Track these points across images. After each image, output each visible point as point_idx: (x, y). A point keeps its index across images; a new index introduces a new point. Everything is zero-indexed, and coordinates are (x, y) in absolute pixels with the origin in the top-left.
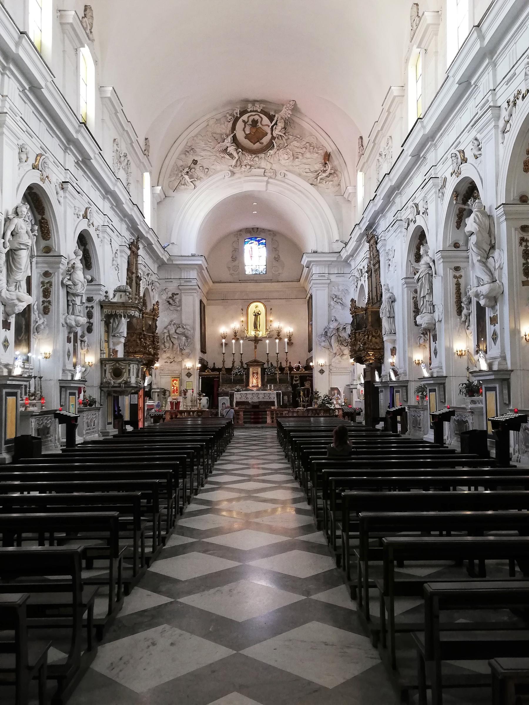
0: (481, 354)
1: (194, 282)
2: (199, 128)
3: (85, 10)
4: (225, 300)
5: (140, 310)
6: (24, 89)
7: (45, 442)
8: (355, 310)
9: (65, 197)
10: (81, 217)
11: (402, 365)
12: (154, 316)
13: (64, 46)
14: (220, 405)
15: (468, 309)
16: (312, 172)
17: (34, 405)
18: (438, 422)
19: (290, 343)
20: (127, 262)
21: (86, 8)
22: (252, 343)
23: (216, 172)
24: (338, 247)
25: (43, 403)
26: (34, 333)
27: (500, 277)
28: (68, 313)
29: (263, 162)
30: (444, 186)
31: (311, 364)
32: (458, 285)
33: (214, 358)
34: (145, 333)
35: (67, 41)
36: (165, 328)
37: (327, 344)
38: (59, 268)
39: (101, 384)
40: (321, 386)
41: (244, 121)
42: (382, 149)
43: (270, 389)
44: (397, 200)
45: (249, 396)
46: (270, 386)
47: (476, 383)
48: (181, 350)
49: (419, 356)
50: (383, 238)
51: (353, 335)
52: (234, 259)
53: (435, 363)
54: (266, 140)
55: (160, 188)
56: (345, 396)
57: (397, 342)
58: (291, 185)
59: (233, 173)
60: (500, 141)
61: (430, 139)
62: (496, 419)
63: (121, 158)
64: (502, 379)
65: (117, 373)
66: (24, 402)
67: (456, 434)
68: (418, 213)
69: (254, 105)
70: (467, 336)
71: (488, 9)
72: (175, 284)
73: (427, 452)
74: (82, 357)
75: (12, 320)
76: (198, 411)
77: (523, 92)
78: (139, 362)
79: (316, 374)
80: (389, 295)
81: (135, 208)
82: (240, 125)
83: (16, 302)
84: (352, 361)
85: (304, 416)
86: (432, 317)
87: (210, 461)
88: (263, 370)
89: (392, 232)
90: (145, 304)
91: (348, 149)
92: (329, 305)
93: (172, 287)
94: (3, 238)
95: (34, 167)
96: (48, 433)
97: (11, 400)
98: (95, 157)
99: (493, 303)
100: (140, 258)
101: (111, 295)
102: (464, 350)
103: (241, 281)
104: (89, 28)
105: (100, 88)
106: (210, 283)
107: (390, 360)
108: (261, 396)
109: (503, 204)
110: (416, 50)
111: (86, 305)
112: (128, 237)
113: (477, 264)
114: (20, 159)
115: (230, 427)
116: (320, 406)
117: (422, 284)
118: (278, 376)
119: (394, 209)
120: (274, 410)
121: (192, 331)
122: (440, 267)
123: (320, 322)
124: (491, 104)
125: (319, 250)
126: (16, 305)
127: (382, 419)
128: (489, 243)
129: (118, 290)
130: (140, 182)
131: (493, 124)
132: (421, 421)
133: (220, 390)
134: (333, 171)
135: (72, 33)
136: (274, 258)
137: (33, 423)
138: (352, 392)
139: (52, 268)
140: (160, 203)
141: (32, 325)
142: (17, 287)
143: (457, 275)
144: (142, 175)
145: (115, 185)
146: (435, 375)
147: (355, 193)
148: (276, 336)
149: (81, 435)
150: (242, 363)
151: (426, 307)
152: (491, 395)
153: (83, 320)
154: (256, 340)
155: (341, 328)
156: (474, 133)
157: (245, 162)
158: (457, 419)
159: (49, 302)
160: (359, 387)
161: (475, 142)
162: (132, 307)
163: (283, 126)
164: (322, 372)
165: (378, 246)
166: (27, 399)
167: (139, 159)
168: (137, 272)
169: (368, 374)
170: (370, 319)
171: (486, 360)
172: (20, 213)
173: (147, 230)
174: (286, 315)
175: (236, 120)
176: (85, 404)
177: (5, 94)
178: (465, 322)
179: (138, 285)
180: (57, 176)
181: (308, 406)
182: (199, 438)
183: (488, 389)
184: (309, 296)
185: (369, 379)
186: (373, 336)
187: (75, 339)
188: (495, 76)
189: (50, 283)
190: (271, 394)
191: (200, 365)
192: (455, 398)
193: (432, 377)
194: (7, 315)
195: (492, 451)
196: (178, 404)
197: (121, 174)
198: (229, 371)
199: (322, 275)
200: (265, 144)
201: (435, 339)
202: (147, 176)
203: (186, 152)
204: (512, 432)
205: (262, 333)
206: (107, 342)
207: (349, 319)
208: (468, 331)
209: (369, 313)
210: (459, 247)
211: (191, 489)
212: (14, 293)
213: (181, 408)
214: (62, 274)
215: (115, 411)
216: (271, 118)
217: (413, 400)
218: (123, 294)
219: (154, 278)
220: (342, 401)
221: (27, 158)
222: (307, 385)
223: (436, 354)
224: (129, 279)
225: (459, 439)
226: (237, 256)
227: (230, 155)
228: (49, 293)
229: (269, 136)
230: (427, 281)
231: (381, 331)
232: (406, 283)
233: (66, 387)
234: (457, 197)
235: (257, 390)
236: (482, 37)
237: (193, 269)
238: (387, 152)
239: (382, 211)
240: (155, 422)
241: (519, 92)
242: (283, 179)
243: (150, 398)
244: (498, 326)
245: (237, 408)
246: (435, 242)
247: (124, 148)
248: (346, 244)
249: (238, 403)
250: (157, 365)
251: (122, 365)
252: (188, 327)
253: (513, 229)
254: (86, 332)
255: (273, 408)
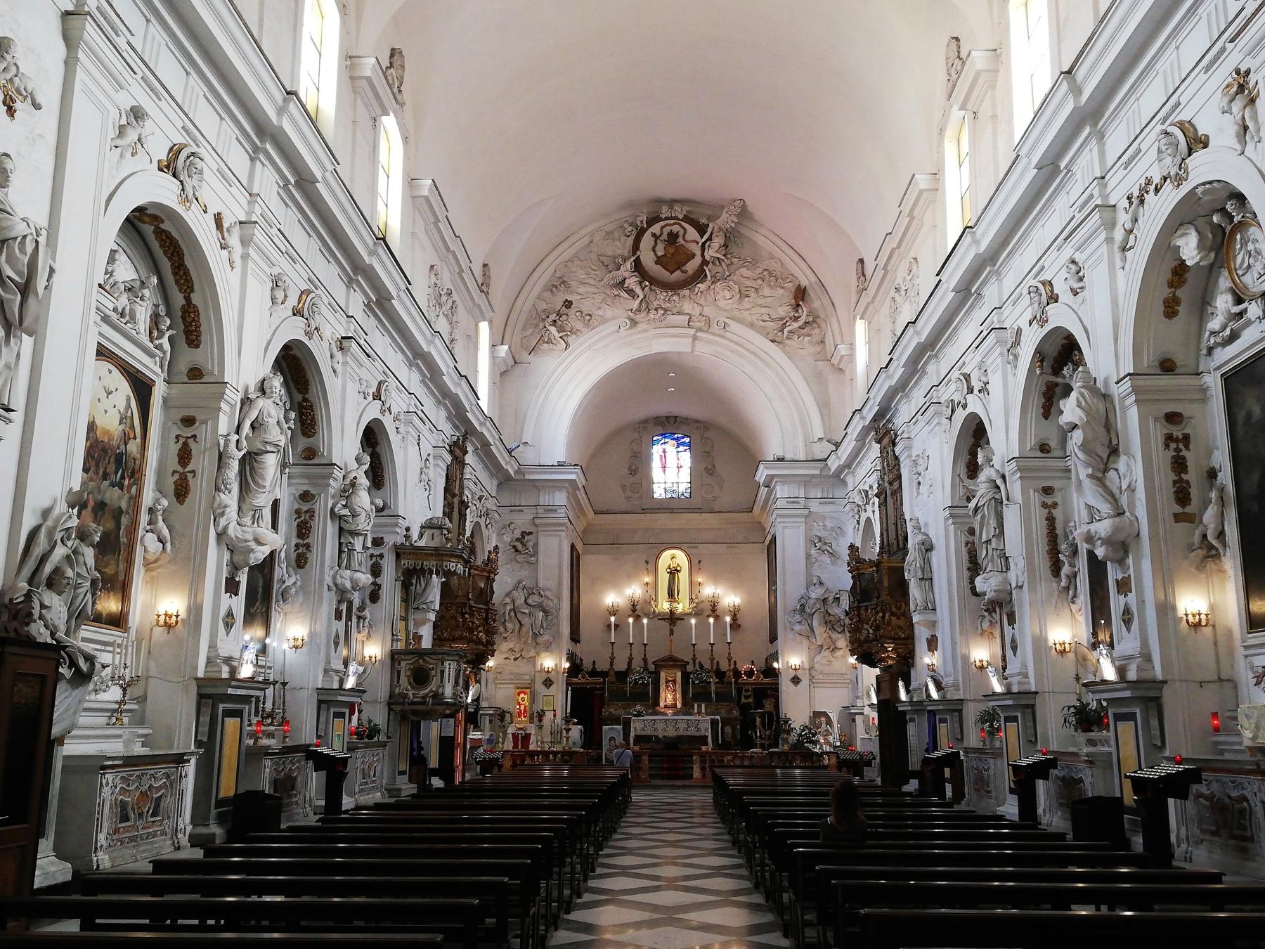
0: (1103, 650)
1: (562, 512)
2: (572, 251)
3: (392, 56)
4: (615, 543)
5: (466, 562)
6: (287, 182)
7: (287, 805)
8: (856, 563)
9: (345, 364)
10: (370, 398)
11: (950, 669)
12: (489, 572)
13: (355, 110)
14: (605, 742)
15: (1072, 565)
16: (773, 320)
17: (270, 735)
18: (1025, 780)
19: (735, 625)
20: (444, 475)
21: (393, 52)
22: (666, 625)
23: (604, 321)
24: (822, 450)
25: (285, 732)
26: (277, 601)
27: (1132, 504)
28: (339, 566)
29: (687, 304)
30: (1017, 343)
31: (775, 665)
32: (1051, 520)
33: (594, 652)
34: (472, 603)
35: (361, 109)
36: (508, 595)
37: (804, 627)
38: (329, 485)
39: (391, 697)
40: (796, 708)
41: (654, 235)
42: (899, 281)
43: (699, 713)
44: (931, 368)
45: (660, 726)
46: (700, 707)
47: (1094, 705)
48: (535, 636)
49: (981, 652)
50: (905, 435)
51: (855, 611)
52: (633, 471)
53: (1014, 666)
54: (691, 266)
55: (506, 347)
56: (841, 729)
57: (940, 625)
58: (736, 343)
59: (634, 323)
60: (1119, 264)
61: (988, 262)
62: (1140, 774)
63: (441, 296)
64: (1145, 697)
65: (420, 677)
66: (254, 728)
67: (1061, 804)
68: (971, 391)
69: (671, 207)
70: (1073, 616)
71: (1086, 45)
72: (528, 515)
73: (1005, 837)
74: (359, 647)
75: (243, 578)
76: (564, 753)
77: (1157, 180)
78: (461, 657)
79: (785, 685)
80: (920, 538)
81: (464, 383)
82: (647, 240)
83: (253, 545)
84: (852, 660)
85: (765, 765)
86: (1005, 579)
87: (591, 849)
88: (686, 676)
89: (921, 424)
90: (473, 551)
91: (840, 282)
92: (808, 556)
93: (522, 521)
94: (237, 432)
95: (296, 312)
96: (293, 788)
97: (232, 723)
98: (399, 296)
99: (1121, 553)
100: (467, 470)
101: (415, 536)
102: (1067, 641)
103: (644, 511)
104: (397, 84)
105: (411, 182)
106: (590, 514)
107: (926, 659)
108: (682, 726)
109: (1129, 374)
110: (957, 114)
111: (371, 551)
112: (448, 431)
113: (1087, 483)
114: (273, 299)
115: (624, 785)
116: (794, 746)
117: (983, 517)
118: (713, 688)
119: (925, 384)
120: (707, 752)
121: (556, 601)
122: (1015, 488)
123: (792, 586)
124: (1099, 202)
125: (788, 456)
126: (252, 550)
127: (914, 775)
128: (1106, 443)
129: (428, 526)
130: (473, 339)
131: (1103, 235)
132: (992, 779)
133: (605, 713)
134: (811, 319)
135: (370, 94)
136: (704, 470)
137: (268, 769)
138: (854, 720)
139: (315, 485)
140: (504, 374)
141: (276, 587)
142: (256, 519)
143: (1049, 501)
144: (477, 325)
145: (430, 342)
146: (1015, 689)
147: (852, 356)
148: (709, 612)
149: (351, 795)
150: (645, 660)
151: (992, 561)
152: (1126, 729)
153: (365, 578)
154: (673, 618)
155: (831, 599)
156: (1068, 252)
157: (655, 303)
158: (1061, 774)
159: (308, 546)
160: (867, 711)
161: (1071, 266)
162: (453, 556)
163: (722, 242)
164: (796, 680)
165: (898, 450)
166: (259, 724)
167: (472, 299)
168: (461, 494)
169: (885, 685)
170: (886, 583)
171: (1113, 662)
172: (268, 391)
173: (370, 242)
174: (730, 574)
175: (641, 233)
176: (360, 735)
177: (255, 191)
178: (1068, 588)
179: (462, 517)
180: (333, 327)
181: (770, 746)
182: (564, 802)
183: (1119, 717)
184: (769, 538)
185: (886, 696)
186: (892, 614)
187: (349, 611)
188: (1102, 154)
189: (311, 513)
190: (702, 722)
191: (567, 665)
192: (1055, 732)
193: (1009, 693)
194: (235, 568)
195: (1133, 839)
196: (527, 737)
197: (442, 325)
198: (622, 676)
199: (793, 500)
200: (690, 272)
201: (1012, 621)
202: (484, 327)
203: (552, 288)
204: (1171, 801)
205: (682, 606)
206: (405, 619)
207: (847, 581)
208: (1073, 607)
209: (885, 571)
210: (1049, 452)
211: (560, 900)
212: (249, 530)
213: (532, 747)
214: (333, 497)
215: (412, 750)
216: (701, 230)
217: (973, 738)
218: (437, 532)
219: (490, 504)
220: (835, 738)
221: (286, 296)
222: (768, 705)
223: (1014, 648)
224: (448, 506)
225: (1068, 816)
226: (638, 468)
227: (630, 292)
228: (309, 529)
229: (697, 260)
230: (993, 513)
231: (908, 604)
232: (952, 516)
233: (330, 702)
234: (1042, 361)
235: (674, 714)
236: (1076, 90)
237: (560, 488)
238: (909, 285)
239: (902, 387)
240: (483, 772)
241: (1149, 182)
242: (721, 332)
243: (477, 728)
244: (1132, 597)
245: (637, 748)
246: (1006, 441)
247: (447, 282)
248: (837, 445)
249: (639, 739)
250: (491, 663)
251: (430, 663)
252: (548, 594)
253: (1151, 421)
254: (368, 601)
255: (704, 748)
